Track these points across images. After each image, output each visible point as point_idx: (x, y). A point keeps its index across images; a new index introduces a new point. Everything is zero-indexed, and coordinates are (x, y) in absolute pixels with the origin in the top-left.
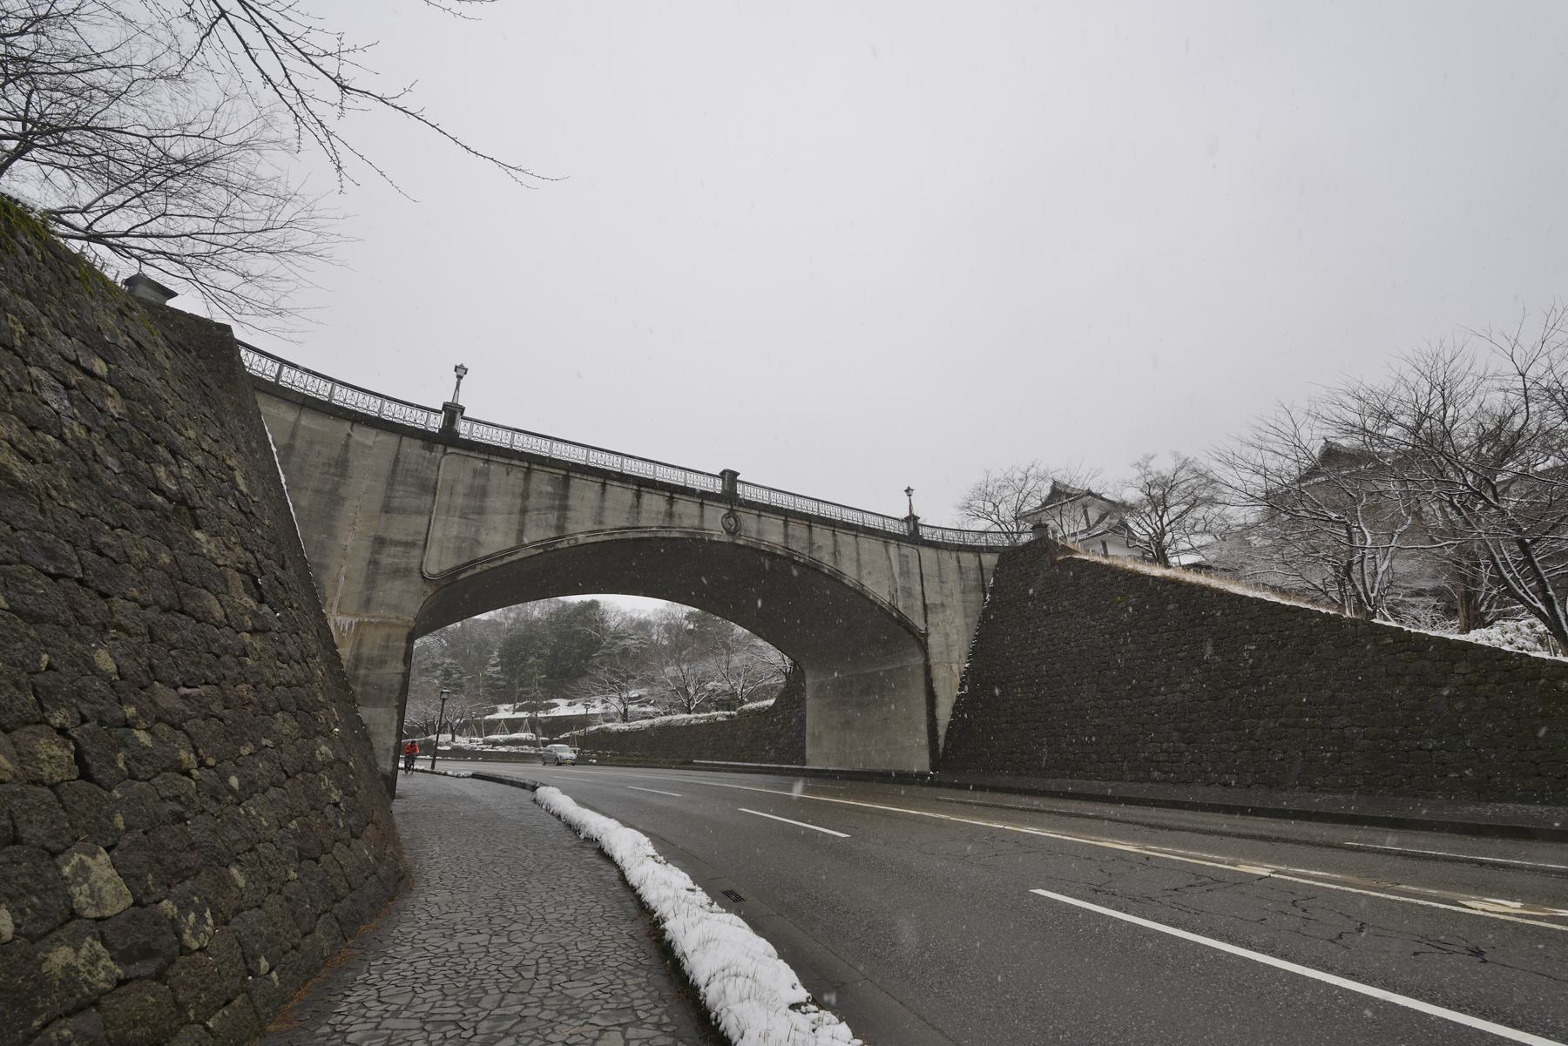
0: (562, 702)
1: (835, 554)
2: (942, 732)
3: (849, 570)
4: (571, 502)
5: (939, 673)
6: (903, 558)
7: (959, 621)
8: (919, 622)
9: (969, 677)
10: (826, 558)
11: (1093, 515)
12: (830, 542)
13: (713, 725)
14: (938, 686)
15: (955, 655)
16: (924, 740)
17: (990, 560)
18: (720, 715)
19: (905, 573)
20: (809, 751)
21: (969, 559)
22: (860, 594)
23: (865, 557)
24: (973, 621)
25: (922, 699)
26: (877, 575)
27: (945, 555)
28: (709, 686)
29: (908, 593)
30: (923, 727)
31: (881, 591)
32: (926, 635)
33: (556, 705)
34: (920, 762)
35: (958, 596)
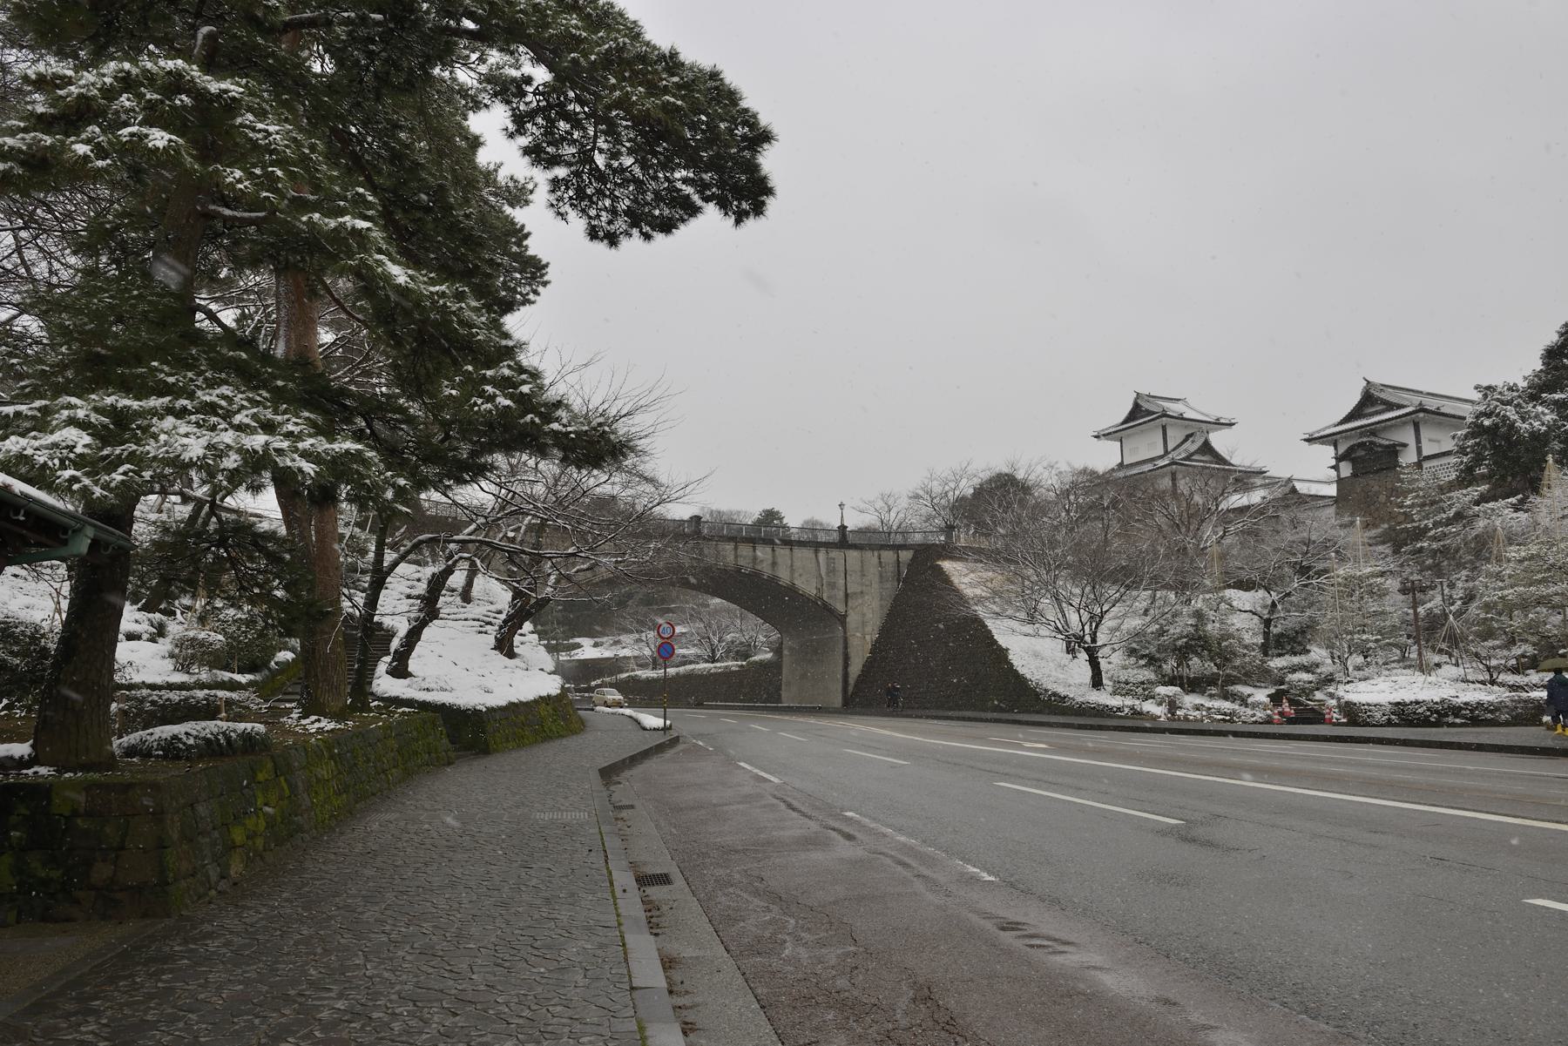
0: (586, 642)
1: (774, 564)
2: (852, 681)
3: (784, 576)
4: (647, 1034)
5: (854, 642)
6: (830, 561)
7: (876, 604)
8: (840, 608)
9: (877, 648)
10: (766, 569)
11: (1175, 436)
12: (769, 556)
13: (727, 674)
14: (852, 652)
15: (868, 629)
16: (839, 686)
17: (906, 556)
18: (733, 665)
19: (831, 571)
20: (784, 694)
21: (888, 556)
22: (792, 590)
23: (797, 564)
24: (888, 604)
25: (841, 662)
26: (802, 573)
27: (869, 554)
28: (729, 637)
29: (832, 586)
30: (839, 676)
31: (808, 586)
32: (845, 616)
33: (579, 646)
34: (838, 701)
35: (876, 586)
